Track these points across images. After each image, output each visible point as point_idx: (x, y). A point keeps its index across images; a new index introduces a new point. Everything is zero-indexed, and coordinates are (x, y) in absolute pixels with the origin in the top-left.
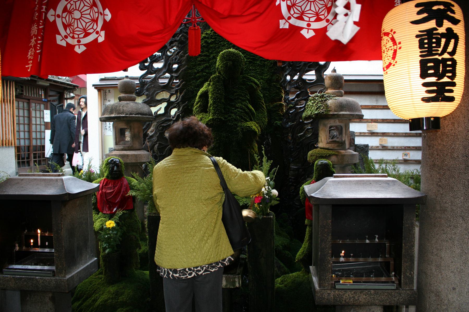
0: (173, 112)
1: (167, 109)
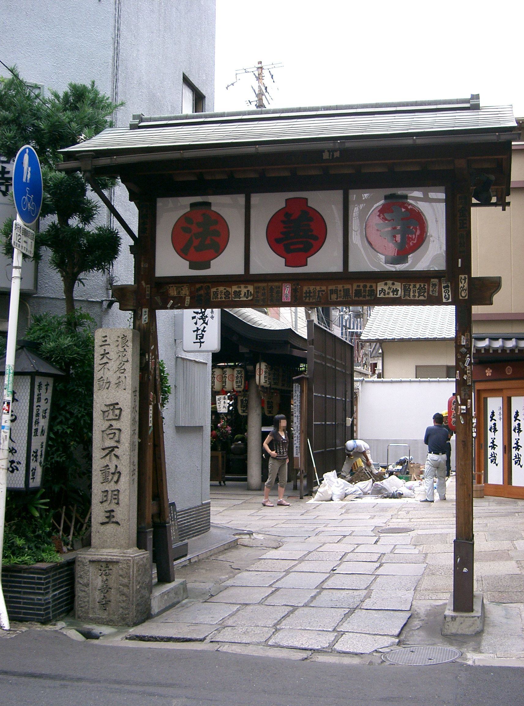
0: (231, 408)
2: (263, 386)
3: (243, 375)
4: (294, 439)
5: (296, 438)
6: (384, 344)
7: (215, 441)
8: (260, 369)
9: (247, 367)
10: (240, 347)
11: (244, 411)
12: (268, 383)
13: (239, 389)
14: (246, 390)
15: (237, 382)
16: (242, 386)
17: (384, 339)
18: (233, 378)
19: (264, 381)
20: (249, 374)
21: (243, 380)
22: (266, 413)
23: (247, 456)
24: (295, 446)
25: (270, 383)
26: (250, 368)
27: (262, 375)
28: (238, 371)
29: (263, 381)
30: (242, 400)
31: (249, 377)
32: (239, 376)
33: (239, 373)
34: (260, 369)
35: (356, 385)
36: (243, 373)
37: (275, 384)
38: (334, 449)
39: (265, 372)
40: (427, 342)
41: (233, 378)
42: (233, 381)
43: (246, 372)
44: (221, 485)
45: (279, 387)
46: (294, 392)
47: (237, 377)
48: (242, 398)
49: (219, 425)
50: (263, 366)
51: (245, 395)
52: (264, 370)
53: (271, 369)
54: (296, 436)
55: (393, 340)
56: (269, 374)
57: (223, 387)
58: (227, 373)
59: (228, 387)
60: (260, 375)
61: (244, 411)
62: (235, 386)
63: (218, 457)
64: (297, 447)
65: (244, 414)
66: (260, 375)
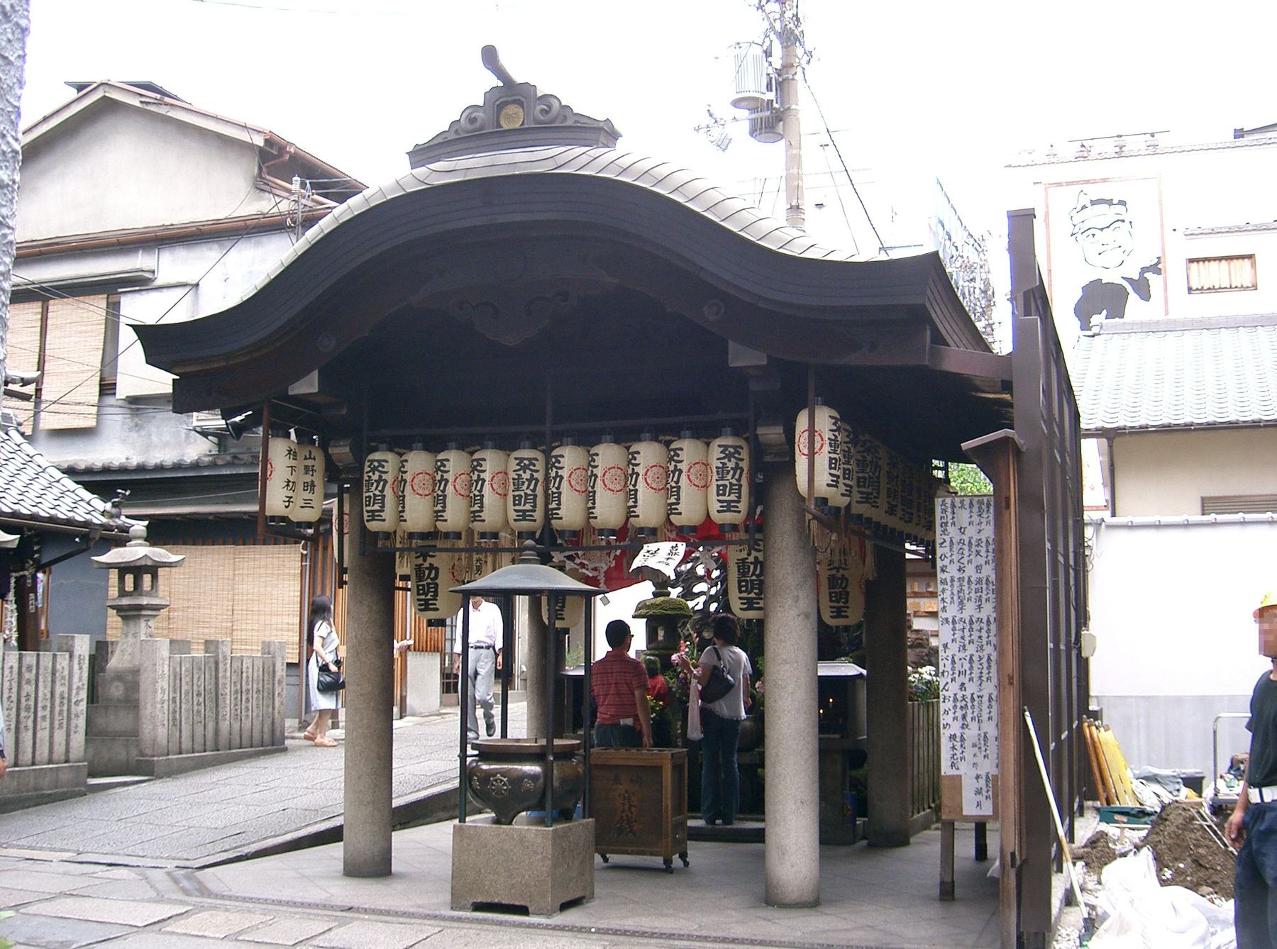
0: (713, 607)
1: (707, 604)
2: (825, 500)
3: (745, 465)
4: (943, 706)
5: (949, 705)
6: (1117, 441)
7: (663, 708)
8: (812, 430)
9: (761, 431)
10: (732, 345)
11: (750, 605)
12: (842, 488)
13: (728, 518)
14: (757, 528)
15: (721, 490)
16: (743, 506)
17: (1119, 428)
18: (705, 476)
19: (828, 479)
20: (768, 459)
21: (744, 482)
22: (828, 620)
23: (762, 756)
24: (945, 734)
25: (848, 493)
26: (771, 433)
27: (818, 456)
28: (726, 447)
29: (823, 477)
30: (742, 563)
31: (770, 470)
32: (731, 465)
33: (729, 457)
34: (812, 430)
35: (1089, 532)
36: (745, 454)
37: (867, 499)
38: (255, 508)
39: (834, 443)
40: (1235, 433)
41: (705, 476)
42: (706, 486)
43: (758, 450)
44: (668, 869)
45: (878, 514)
46: (938, 530)
47: (722, 472)
48: (744, 554)
49: (674, 657)
50: (825, 419)
51: (753, 545)
52: (827, 435)
53: (854, 441)
54: (950, 694)
55: (1143, 431)
56: (847, 454)
57: (671, 509)
58: (683, 455)
59: (689, 512)
60: (812, 455)
61: (750, 605)
62: (715, 506)
63: (658, 770)
64: (953, 737)
65: (752, 614)
66: (812, 455)
